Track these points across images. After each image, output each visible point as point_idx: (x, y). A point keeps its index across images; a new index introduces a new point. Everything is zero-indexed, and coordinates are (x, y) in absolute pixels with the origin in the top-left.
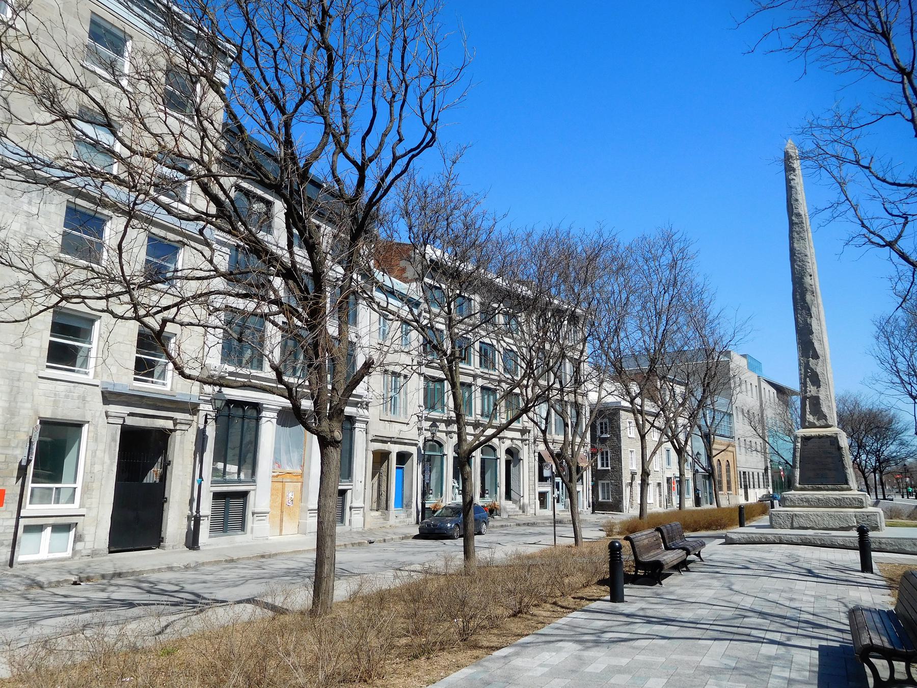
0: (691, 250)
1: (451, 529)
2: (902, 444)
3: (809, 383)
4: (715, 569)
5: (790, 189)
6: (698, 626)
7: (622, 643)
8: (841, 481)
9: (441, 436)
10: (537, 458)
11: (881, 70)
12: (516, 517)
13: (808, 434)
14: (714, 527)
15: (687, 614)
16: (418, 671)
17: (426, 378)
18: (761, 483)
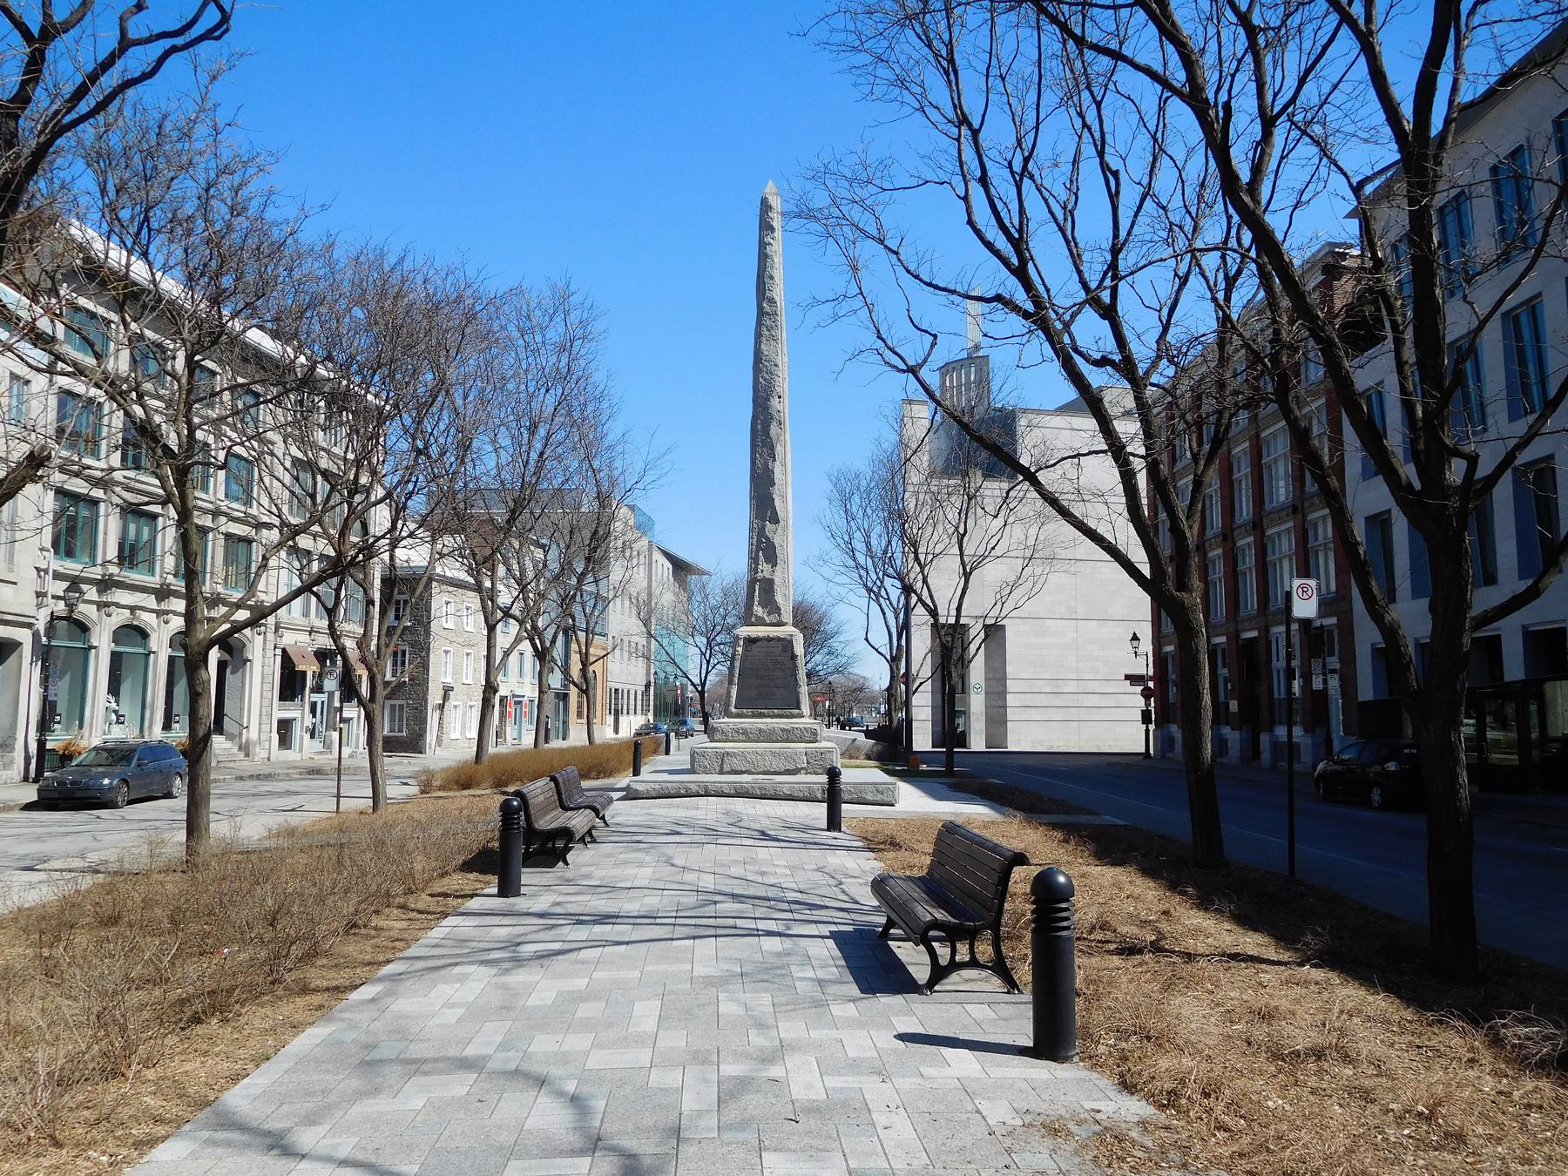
0: (596, 327)
1: (111, 788)
2: (830, 653)
3: (762, 558)
4: (634, 837)
5: (763, 257)
6: (658, 921)
7: (560, 957)
8: (791, 704)
9: (87, 611)
10: (279, 659)
11: (934, 115)
12: (232, 765)
13: (753, 635)
14: (593, 774)
15: (632, 906)
16: (215, 1044)
17: (60, 492)
18: (639, 707)
